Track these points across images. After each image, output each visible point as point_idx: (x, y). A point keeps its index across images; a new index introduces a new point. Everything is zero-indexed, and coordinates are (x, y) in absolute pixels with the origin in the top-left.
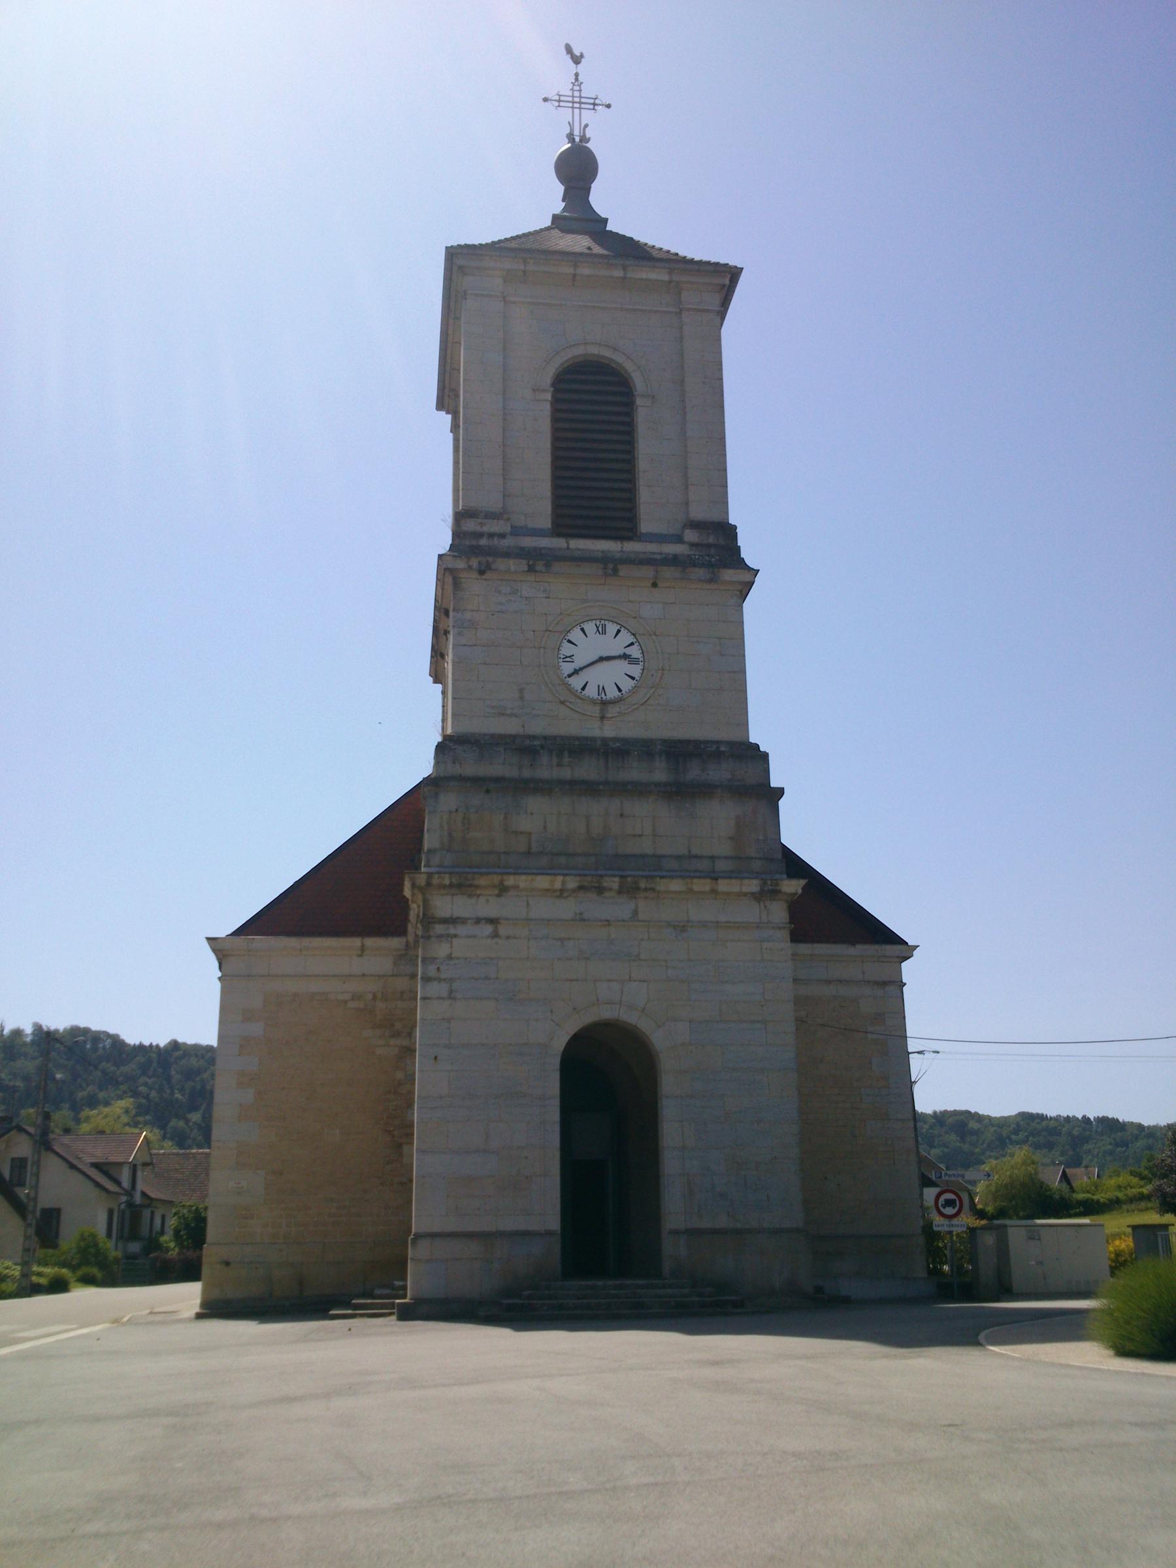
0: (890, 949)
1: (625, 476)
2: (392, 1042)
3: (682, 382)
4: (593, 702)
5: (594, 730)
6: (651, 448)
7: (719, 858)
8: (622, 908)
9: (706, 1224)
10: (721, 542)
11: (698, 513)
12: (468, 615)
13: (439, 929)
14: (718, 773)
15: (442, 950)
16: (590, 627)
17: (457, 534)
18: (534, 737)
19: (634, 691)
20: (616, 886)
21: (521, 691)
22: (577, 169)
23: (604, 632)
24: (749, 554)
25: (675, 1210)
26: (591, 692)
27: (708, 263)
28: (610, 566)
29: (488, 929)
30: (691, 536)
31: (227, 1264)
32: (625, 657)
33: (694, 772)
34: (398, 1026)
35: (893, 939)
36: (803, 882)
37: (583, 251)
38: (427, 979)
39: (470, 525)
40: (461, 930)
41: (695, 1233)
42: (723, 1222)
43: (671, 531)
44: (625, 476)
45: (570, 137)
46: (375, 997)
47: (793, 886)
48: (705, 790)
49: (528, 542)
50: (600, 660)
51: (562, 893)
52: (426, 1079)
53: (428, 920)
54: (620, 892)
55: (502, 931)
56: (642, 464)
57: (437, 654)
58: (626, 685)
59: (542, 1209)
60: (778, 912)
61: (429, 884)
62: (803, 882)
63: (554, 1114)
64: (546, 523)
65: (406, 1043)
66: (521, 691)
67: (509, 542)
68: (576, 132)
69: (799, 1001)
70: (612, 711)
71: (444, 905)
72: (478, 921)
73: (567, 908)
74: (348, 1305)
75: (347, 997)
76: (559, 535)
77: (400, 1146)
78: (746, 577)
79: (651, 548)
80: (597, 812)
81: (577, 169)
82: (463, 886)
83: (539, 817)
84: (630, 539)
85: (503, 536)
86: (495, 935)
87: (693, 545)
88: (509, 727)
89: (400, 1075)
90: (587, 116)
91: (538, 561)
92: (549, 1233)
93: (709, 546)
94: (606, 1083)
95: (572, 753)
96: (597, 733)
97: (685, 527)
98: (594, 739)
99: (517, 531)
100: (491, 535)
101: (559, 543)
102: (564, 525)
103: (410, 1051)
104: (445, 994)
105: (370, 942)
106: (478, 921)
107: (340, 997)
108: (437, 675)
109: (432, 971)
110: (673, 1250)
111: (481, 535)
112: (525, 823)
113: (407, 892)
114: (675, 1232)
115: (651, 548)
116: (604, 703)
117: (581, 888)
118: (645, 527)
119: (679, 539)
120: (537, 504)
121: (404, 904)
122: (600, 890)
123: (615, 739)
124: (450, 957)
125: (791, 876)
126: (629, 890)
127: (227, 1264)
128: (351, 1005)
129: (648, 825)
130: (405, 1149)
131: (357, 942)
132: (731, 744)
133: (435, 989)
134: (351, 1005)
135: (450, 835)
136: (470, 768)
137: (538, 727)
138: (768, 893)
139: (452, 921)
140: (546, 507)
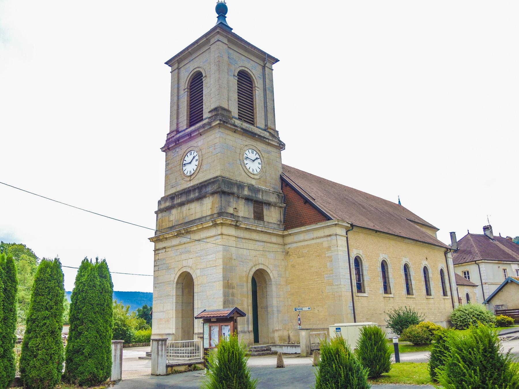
29: (164, 250)
86: (166, 251)
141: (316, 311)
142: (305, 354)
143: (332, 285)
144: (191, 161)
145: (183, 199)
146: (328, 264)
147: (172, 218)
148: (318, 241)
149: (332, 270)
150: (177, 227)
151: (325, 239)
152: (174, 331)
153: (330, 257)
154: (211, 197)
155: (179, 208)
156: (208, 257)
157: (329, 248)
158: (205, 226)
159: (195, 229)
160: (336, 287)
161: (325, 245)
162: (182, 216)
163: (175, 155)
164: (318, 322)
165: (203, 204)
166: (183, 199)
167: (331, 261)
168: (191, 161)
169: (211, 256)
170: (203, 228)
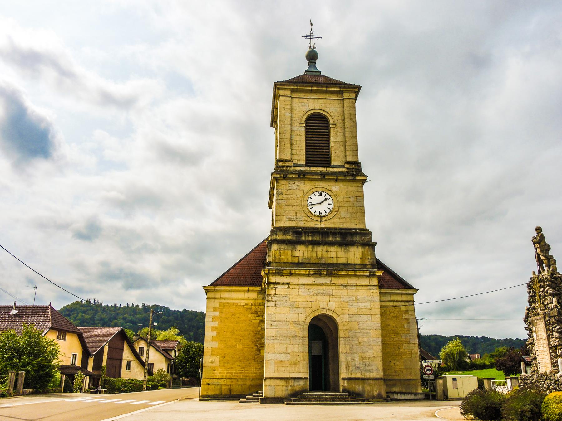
0: (410, 291)
1: (327, 148)
2: (257, 318)
3: (344, 120)
4: (318, 216)
5: (318, 225)
6: (335, 139)
7: (357, 264)
8: (327, 281)
9: (353, 376)
10: (356, 167)
11: (349, 159)
12: (280, 191)
13: (272, 286)
14: (357, 239)
15: (272, 292)
16: (317, 194)
17: (277, 166)
18: (300, 228)
19: (330, 213)
20: (325, 273)
21: (296, 213)
22: (312, 57)
23: (321, 195)
24: (365, 171)
25: (343, 373)
26: (317, 214)
27: (352, 85)
28: (323, 177)
29: (287, 286)
30: (347, 166)
31: (209, 384)
32: (326, 199)
33: (349, 238)
34: (259, 313)
35: (407, 286)
36: (382, 272)
37: (311, 81)
38: (268, 301)
39: (281, 164)
40: (278, 286)
41: (349, 379)
42: (358, 376)
43: (341, 164)
44: (327, 148)
45: (310, 47)
46: (252, 305)
47: (380, 273)
48: (352, 244)
49: (298, 168)
50: (320, 204)
51: (309, 275)
52: (269, 332)
53: (269, 284)
54: (326, 275)
55: (291, 287)
56: (332, 144)
57: (271, 200)
58: (312, 196)
59: (302, 371)
60: (375, 281)
61: (269, 272)
62: (382, 272)
63: (307, 342)
64: (303, 162)
65: (261, 319)
66: (296, 213)
67: (292, 168)
68: (312, 46)
69: (381, 307)
70: (324, 219)
71: (273, 279)
72: (283, 284)
73: (310, 280)
74: (245, 398)
75: (244, 304)
76: (307, 166)
77: (260, 350)
78: (364, 178)
79: (335, 169)
80: (320, 251)
81: (312, 57)
82: (279, 273)
83: (301, 252)
84: (329, 167)
85: (291, 167)
86: (289, 288)
87: (347, 169)
88: (292, 224)
89: (259, 328)
90: (315, 41)
91: (302, 176)
92: (306, 378)
93: (353, 169)
94: (322, 334)
95: (312, 232)
96: (319, 226)
97: (346, 163)
98: (318, 228)
99: (295, 165)
100: (287, 167)
101: (308, 168)
102: (309, 163)
103: (263, 321)
104: (274, 305)
105: (250, 288)
106: (283, 284)
107: (242, 304)
108: (271, 207)
109: (270, 298)
110: (343, 384)
111: (284, 167)
112: (297, 253)
113: (262, 274)
114: (344, 379)
115: (335, 169)
116: (321, 217)
117: (314, 274)
118: (333, 163)
119: (343, 167)
120: (300, 158)
121: (261, 278)
122: (321, 275)
123: (325, 228)
124: (275, 294)
125: (379, 269)
126: (330, 274)
127: (209, 384)
128: (245, 307)
129: (336, 254)
130: (261, 351)
131: (246, 288)
132: (360, 229)
133: (270, 304)
134: (245, 307)
135: (275, 257)
136: (280, 237)
137: (301, 224)
138: (372, 275)
139: (276, 284)
140: (303, 158)
141: (392, 364)
142: (442, 399)
143: (409, 343)
144: (322, 202)
145: (317, 238)
146: (405, 325)
147: (297, 253)
148: (395, 304)
149: (409, 331)
150: (309, 265)
151: (403, 304)
152: (307, 376)
153: (407, 319)
154: (360, 248)
155: (310, 247)
156: (360, 304)
157: (406, 312)
158: (358, 274)
159: (343, 273)
160: (413, 345)
161: (403, 308)
162: (314, 255)
163: (293, 188)
164: (394, 374)
165: (348, 251)
166: (317, 238)
167: (409, 323)
168: (322, 202)
169: (364, 304)
170: (355, 276)
